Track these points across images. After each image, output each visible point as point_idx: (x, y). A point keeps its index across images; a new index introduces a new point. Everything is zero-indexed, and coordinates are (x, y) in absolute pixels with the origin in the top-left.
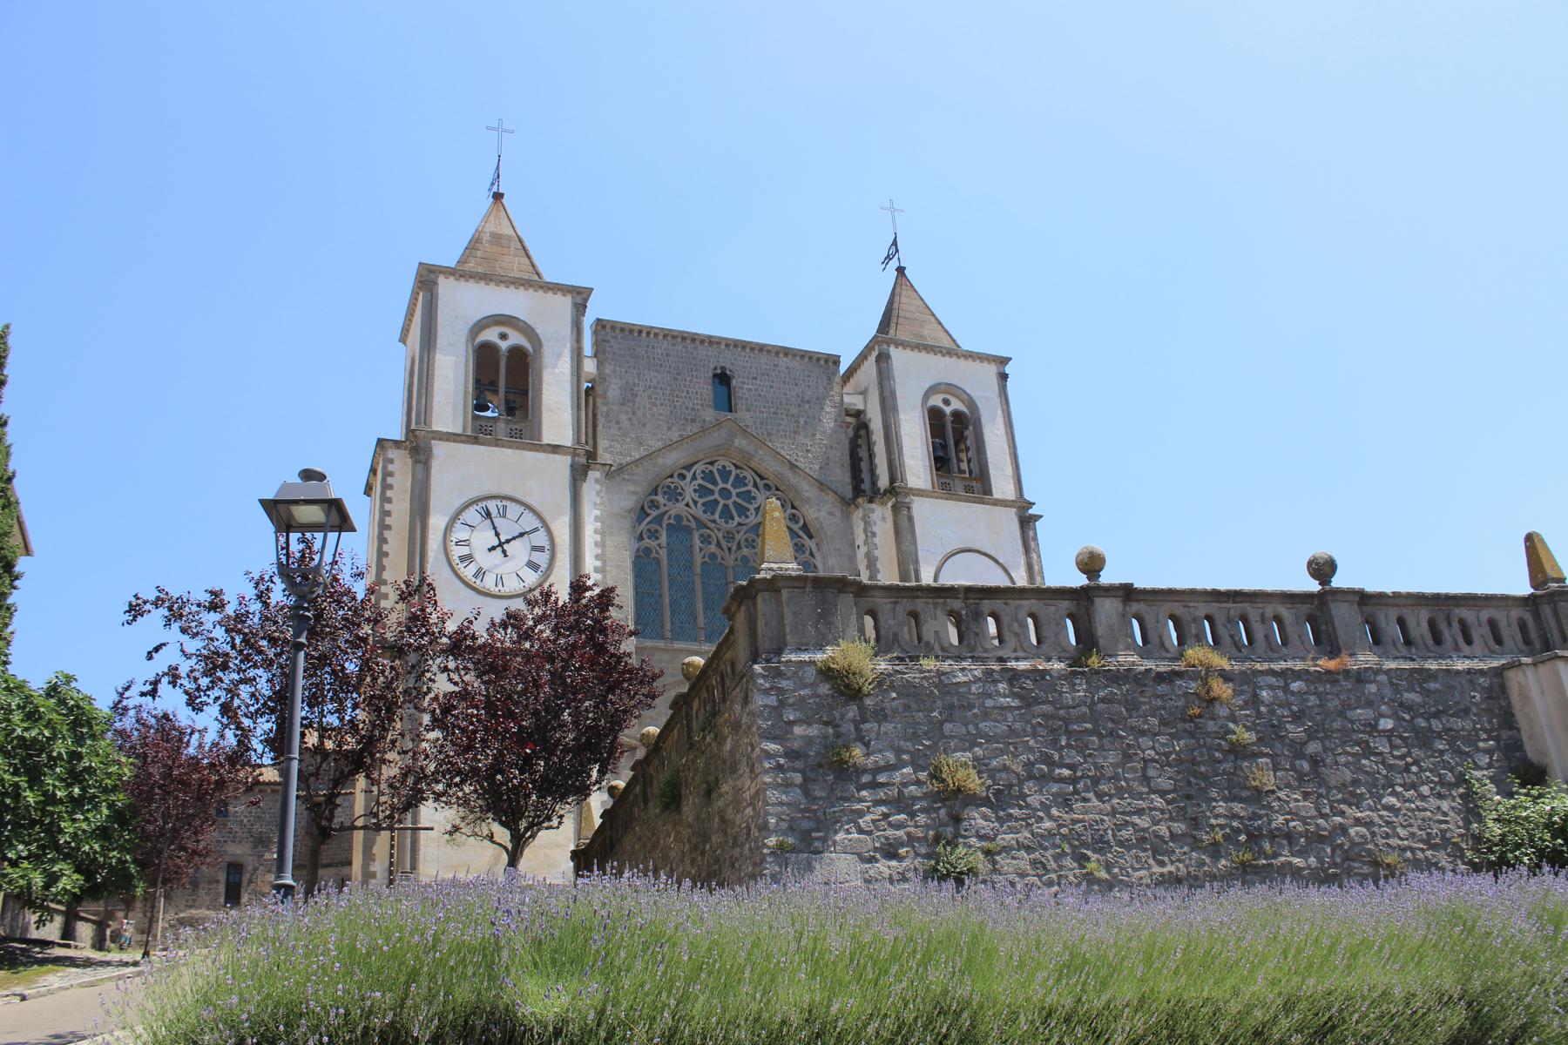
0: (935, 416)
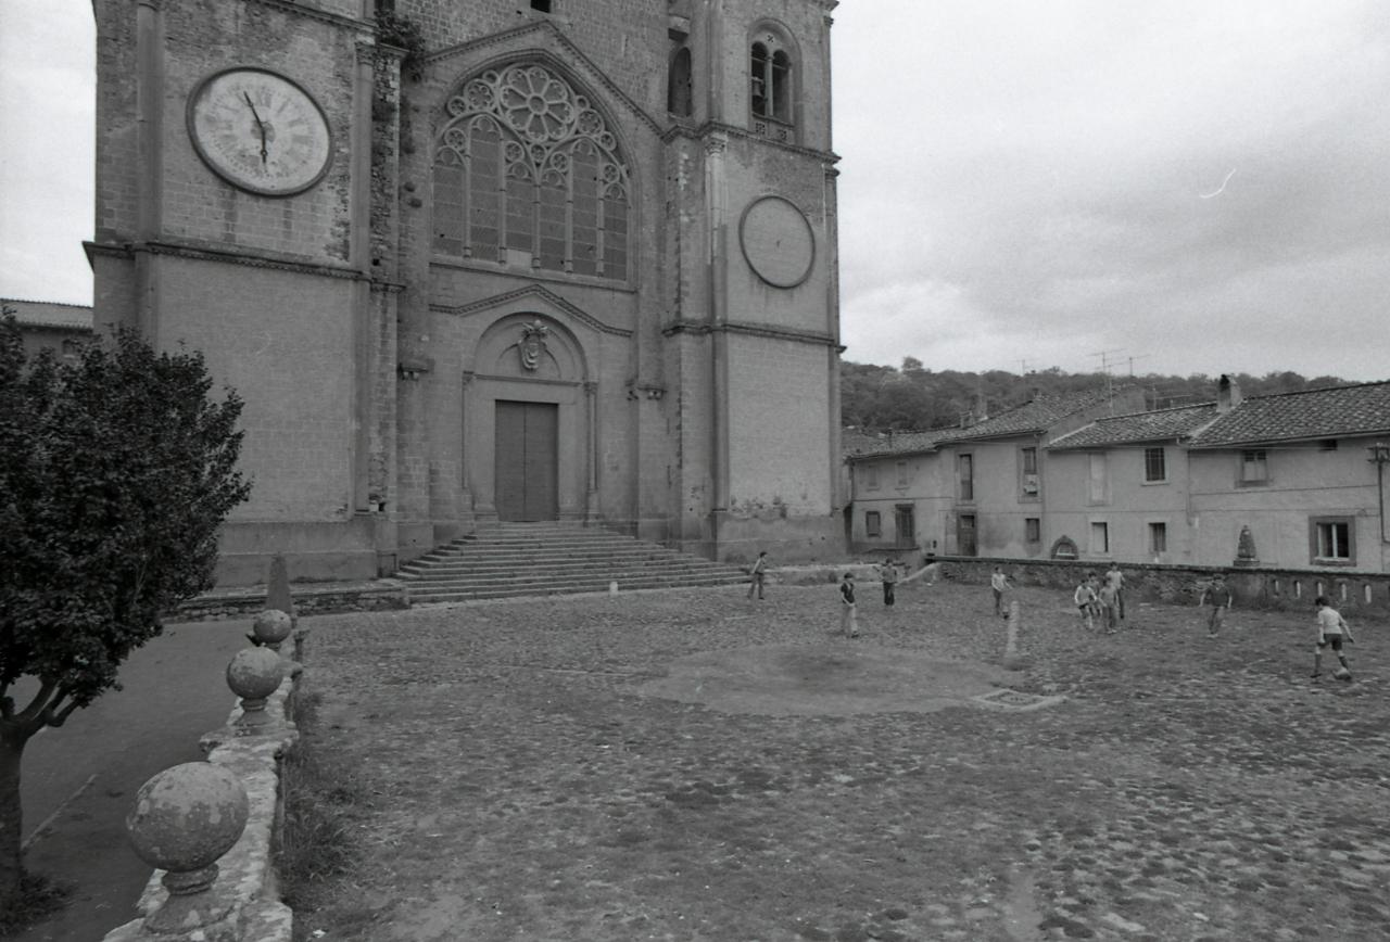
0: (758, 51)
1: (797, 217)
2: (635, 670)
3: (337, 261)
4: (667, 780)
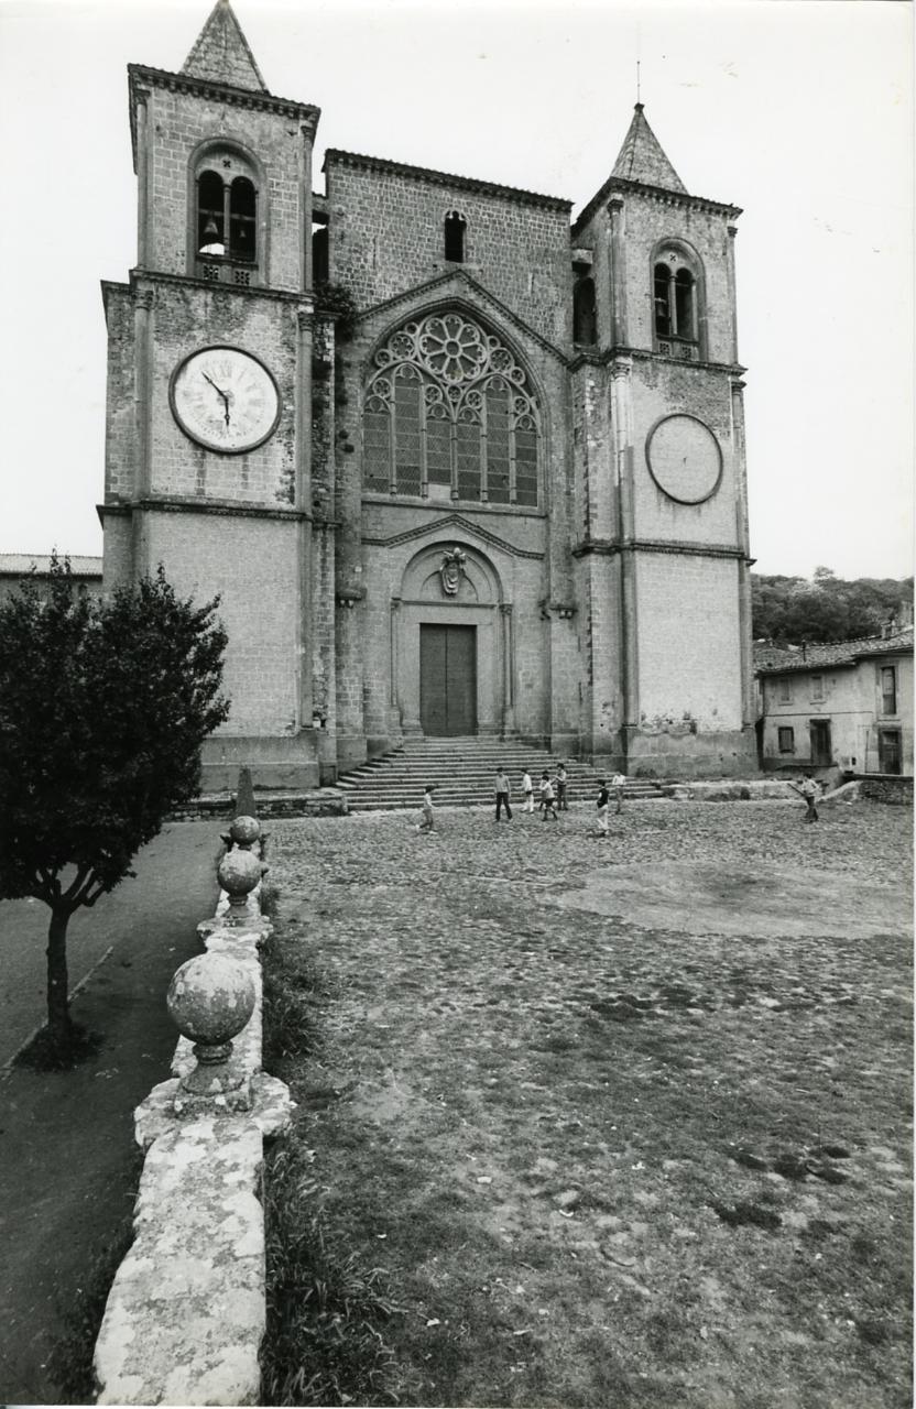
0: (661, 272)
1: (704, 432)
2: (554, 881)
3: (285, 505)
4: (591, 990)
